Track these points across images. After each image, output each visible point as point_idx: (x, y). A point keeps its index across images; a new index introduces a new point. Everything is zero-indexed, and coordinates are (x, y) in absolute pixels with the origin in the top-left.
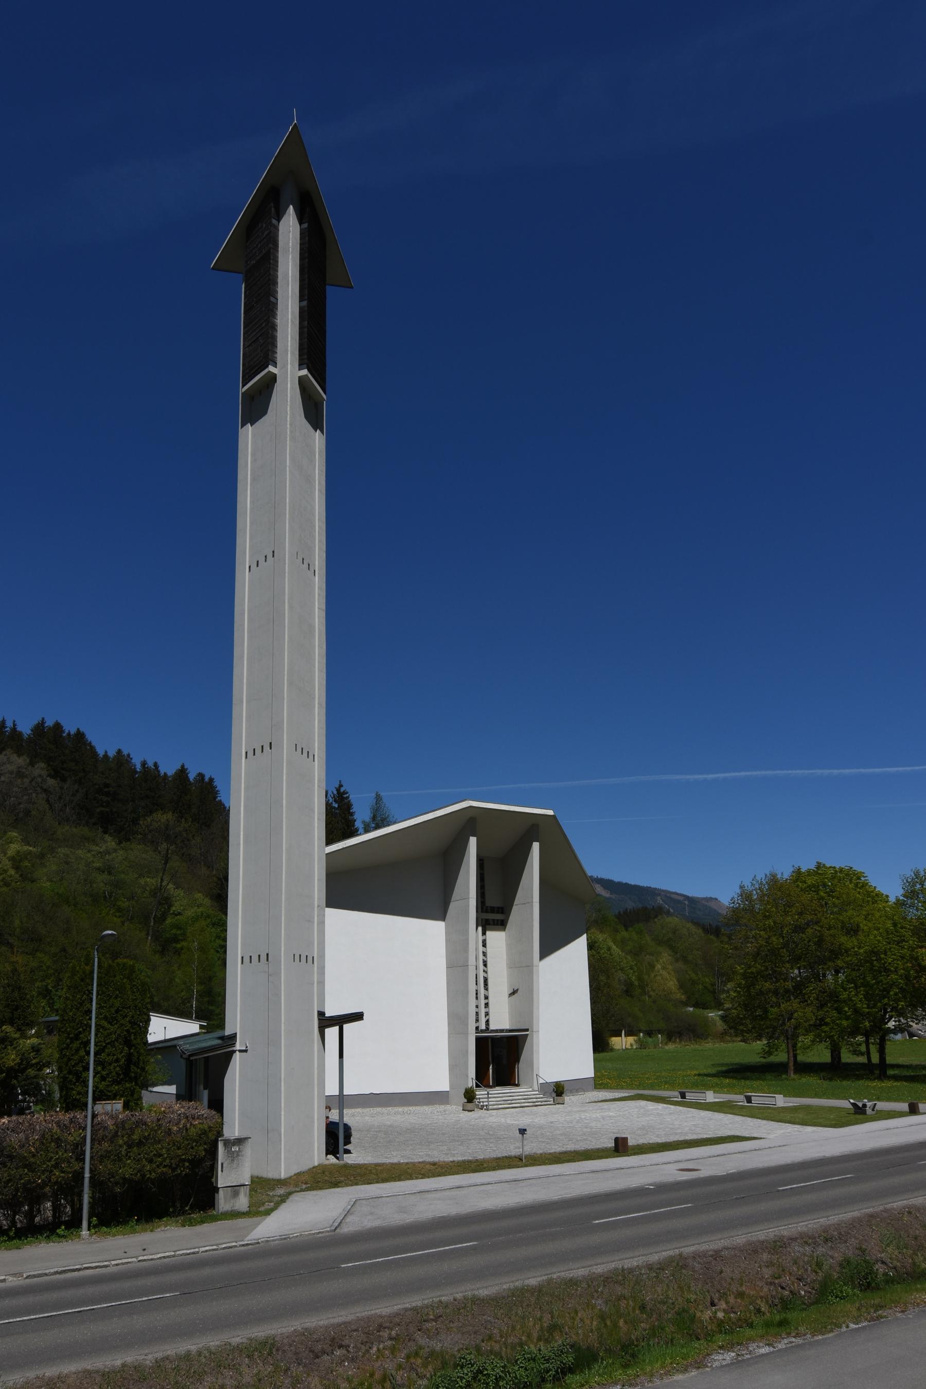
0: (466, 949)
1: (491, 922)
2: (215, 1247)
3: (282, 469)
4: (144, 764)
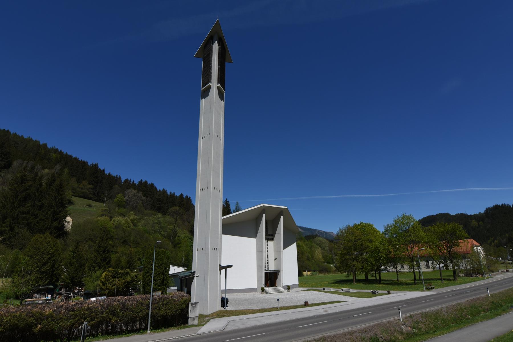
0: (262, 247)
3: (212, 111)
4: (171, 193)
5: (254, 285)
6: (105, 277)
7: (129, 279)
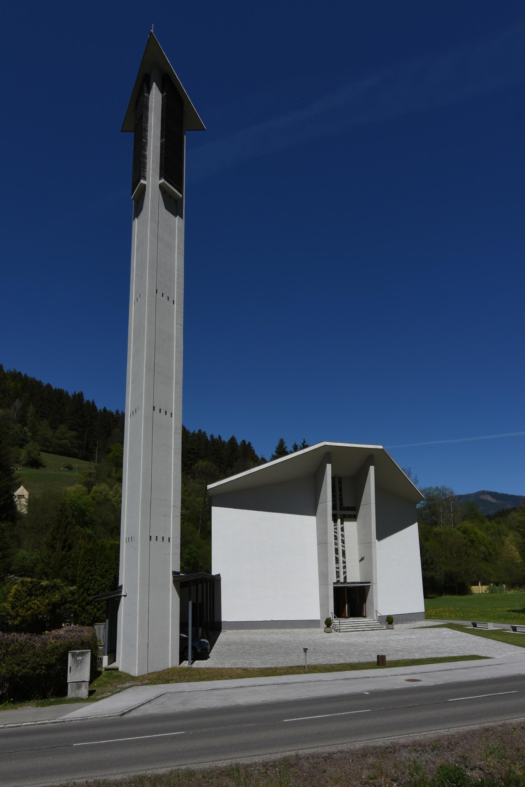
0: (326, 533)
1: (347, 516)
2: (33, 723)
3: (157, 244)
4: (212, 436)
5: (314, 613)
6: (15, 594)
7: (56, 597)
